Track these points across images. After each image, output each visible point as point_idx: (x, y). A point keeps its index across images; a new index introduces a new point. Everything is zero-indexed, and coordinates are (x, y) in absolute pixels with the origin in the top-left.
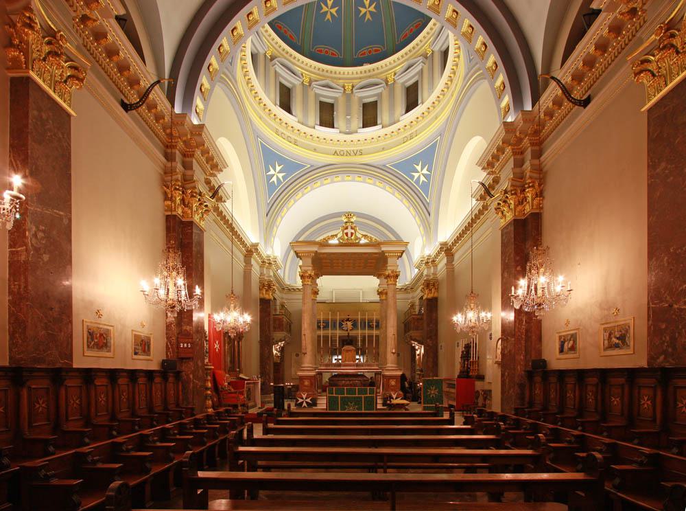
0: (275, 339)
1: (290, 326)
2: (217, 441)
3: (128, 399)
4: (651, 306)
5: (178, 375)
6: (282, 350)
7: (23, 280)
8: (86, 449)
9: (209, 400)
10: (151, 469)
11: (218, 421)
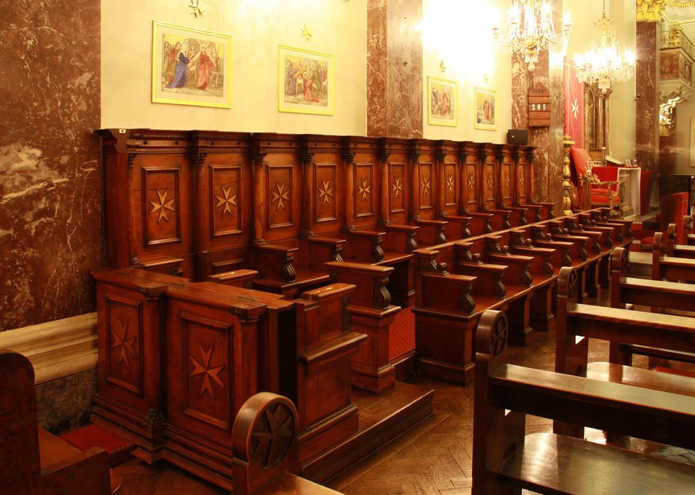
0: (663, 95)
1: (690, 68)
2: (598, 256)
3: (475, 186)
4: (619, 169)
5: (529, 151)
6: (673, 114)
7: (381, 30)
8: (464, 242)
9: (566, 196)
10: (531, 281)
11: (552, 242)
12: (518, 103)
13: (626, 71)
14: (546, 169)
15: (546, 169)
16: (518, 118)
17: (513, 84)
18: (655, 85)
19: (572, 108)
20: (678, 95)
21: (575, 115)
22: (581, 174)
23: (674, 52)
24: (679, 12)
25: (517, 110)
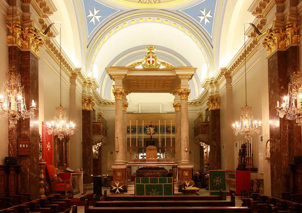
1: (106, 131)
6: (100, 149)
9: (42, 188)
12: (12, 144)
13: (71, 131)
14: (28, 176)
15: (28, 176)
16: (12, 151)
17: (9, 133)
18: (90, 137)
19: (47, 146)
20: (101, 142)
21: (49, 149)
22: (51, 177)
23: (99, 124)
24: (101, 108)
25: (11, 147)
